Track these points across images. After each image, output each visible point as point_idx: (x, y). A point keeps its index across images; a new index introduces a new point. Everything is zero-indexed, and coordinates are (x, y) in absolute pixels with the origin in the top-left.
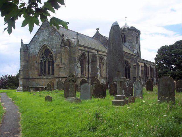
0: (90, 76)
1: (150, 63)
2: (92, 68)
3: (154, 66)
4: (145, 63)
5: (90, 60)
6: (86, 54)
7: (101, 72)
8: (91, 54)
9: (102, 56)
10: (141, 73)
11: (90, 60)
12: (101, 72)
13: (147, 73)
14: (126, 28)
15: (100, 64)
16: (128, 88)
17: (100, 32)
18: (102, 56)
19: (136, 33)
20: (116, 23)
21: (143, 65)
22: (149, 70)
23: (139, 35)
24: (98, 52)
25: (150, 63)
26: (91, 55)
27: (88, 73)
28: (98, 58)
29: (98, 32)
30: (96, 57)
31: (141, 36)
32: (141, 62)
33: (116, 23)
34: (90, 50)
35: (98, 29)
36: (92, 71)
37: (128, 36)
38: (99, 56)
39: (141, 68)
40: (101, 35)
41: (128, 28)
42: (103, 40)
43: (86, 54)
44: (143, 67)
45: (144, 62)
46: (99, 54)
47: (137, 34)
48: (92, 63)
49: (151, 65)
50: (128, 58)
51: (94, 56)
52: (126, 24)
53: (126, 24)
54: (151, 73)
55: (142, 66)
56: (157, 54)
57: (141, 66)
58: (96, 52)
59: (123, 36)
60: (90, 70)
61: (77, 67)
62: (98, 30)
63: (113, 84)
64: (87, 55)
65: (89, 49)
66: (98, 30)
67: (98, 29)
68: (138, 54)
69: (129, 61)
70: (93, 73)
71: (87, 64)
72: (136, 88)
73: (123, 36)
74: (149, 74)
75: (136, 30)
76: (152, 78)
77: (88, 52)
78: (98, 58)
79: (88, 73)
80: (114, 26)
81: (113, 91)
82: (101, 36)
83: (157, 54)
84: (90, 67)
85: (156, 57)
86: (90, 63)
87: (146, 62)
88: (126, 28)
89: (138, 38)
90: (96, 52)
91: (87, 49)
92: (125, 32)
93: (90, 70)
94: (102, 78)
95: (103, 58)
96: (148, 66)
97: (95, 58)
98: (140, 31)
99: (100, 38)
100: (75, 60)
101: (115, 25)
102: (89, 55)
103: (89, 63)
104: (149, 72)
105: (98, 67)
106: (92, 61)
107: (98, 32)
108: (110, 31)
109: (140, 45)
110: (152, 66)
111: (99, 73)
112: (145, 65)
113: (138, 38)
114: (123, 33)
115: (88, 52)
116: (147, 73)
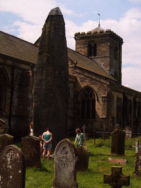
0: (14, 113)
1: (134, 94)
4: (124, 94)
6: (9, 71)
8: (19, 71)
10: (116, 112)
14: (98, 31)
16: (11, 170)
20: (57, 10)
21: (121, 96)
25: (134, 94)
26: (18, 74)
27: (11, 107)
32: (116, 91)
41: (102, 32)
43: (9, 71)
44: (120, 99)
47: (116, 43)
49: (136, 96)
50: (94, 84)
52: (99, 25)
53: (99, 25)
57: (115, 99)
59: (93, 45)
60: (16, 101)
68: (116, 77)
69: (95, 88)
72: (60, 159)
73: (93, 45)
74: (131, 112)
77: (13, 68)
79: (11, 107)
80: (52, 16)
84: (15, 96)
88: (98, 31)
91: (9, 62)
92: (96, 39)
93: (16, 101)
98: (122, 40)
101: (53, 13)
103: (12, 89)
108: (45, 26)
113: (118, 50)
114: (92, 39)
115: (13, 68)
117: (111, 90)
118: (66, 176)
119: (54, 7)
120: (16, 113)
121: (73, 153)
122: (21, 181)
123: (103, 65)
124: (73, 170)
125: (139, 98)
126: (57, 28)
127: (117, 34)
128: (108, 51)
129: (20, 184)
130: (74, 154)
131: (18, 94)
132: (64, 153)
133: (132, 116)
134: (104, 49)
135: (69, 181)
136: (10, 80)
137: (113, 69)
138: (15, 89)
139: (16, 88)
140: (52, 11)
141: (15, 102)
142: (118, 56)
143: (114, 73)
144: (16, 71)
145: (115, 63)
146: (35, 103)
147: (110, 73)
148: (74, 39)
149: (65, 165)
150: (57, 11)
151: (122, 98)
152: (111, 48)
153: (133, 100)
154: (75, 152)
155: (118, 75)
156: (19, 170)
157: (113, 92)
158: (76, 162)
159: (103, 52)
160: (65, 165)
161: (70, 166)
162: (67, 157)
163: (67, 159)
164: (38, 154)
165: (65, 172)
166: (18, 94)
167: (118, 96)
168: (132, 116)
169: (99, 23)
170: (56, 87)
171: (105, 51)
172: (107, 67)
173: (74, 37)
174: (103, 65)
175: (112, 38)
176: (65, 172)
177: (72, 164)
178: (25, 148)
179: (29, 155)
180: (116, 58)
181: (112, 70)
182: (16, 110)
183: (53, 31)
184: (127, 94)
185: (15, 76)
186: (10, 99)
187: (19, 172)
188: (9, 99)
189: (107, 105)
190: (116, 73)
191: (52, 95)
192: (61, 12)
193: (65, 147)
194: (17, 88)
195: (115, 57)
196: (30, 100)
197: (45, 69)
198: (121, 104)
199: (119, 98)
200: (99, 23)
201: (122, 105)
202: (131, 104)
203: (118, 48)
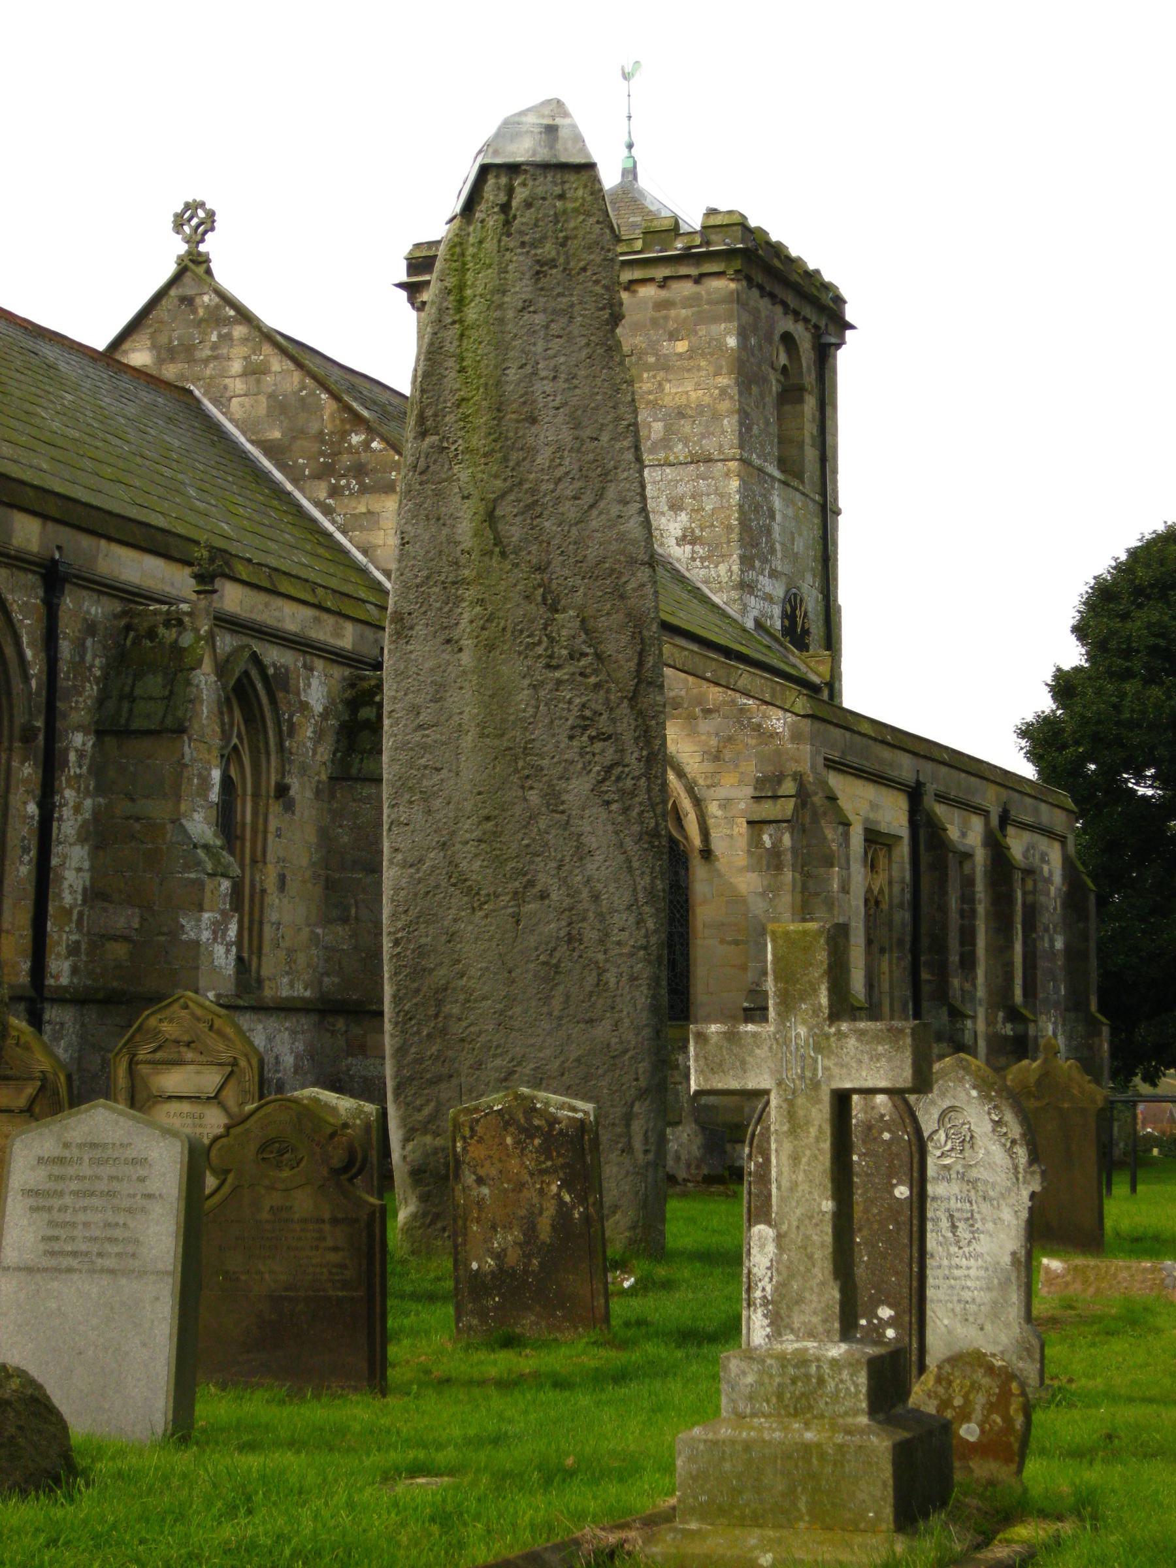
0: (60, 971)
1: (990, 798)
2: (99, 834)
3: (1043, 843)
4: (914, 794)
5: (80, 706)
7: (246, 902)
8: (97, 609)
9: (274, 656)
11: (80, 706)
12: (246, 902)
13: (954, 944)
15: (227, 784)
17: (233, 270)
18: (274, 656)
19: (787, 324)
21: (893, 814)
22: (968, 899)
23: (825, 356)
24: (206, 580)
25: (990, 798)
26: (91, 628)
28: (205, 680)
29: (194, 266)
30: (178, 665)
31: (848, 361)
33: (551, 130)
34: (86, 541)
35: (195, 221)
36: (95, 895)
37: (664, 365)
38: (226, 642)
39: (858, 873)
40: (245, 316)
42: (279, 407)
45: (905, 767)
46: (227, 622)
48: (97, 770)
51: (142, 646)
54: (1009, 946)
55: (875, 839)
56: (1073, 655)
58: (170, 579)
60: (74, 865)
61: (718, 789)
62: (195, 240)
63: (506, 1119)
64: (28, 625)
65: (64, 535)
66: (195, 240)
67: (195, 221)
70: (125, 919)
71: (27, 771)
74: (968, 963)
75: (770, 271)
76: (1014, 1015)
77: (54, 577)
78: (205, 680)
80: (513, 169)
81: (507, 1239)
82: (239, 331)
83: (1073, 655)
84: (68, 825)
85: (1045, 704)
86: (74, 766)
87: (936, 779)
89: (810, 402)
90: (170, 579)
94: (262, 1009)
95: (278, 683)
96: (967, 833)
97: (153, 684)
98: (839, 301)
99: (236, 367)
100: (769, 531)
101: (521, 151)
102: (68, 628)
103: (51, 764)
104: (968, 936)
105: (200, 825)
106: (110, 730)
107: (194, 266)
109: (826, 511)
110: (1017, 844)
111: (219, 929)
112: (925, 831)
113: (810, 402)
115: (54, 577)
116: (940, 946)
117: (820, 761)
118: (967, 1295)
119: (520, 96)
120: (75, 970)
121: (1014, 1142)
122: (911, 1241)
123: (682, 540)
124: (1014, 1254)
125: (1027, 836)
126: (552, 263)
127: (794, 252)
128: (725, 406)
129: (906, 1256)
130: (1021, 1152)
131: (88, 803)
132: (952, 1149)
133: (981, 993)
134: (684, 390)
135: (988, 1327)
136: (34, 683)
137: (774, 574)
138: (66, 762)
139: (72, 756)
140: (509, 129)
141: (70, 876)
142: (811, 454)
143: (777, 611)
144: (82, 608)
145: (785, 516)
146: (405, 865)
147: (744, 610)
148: (404, 294)
149: (954, 1227)
150: (551, 130)
151: (904, 833)
152: (747, 376)
153: (980, 856)
154: (1023, 1135)
155: (811, 625)
156: (895, 1186)
157: (835, 781)
158: (1033, 1196)
159: (681, 415)
160: (954, 1227)
161: (990, 1226)
162: (974, 1173)
163: (973, 1183)
164: (586, 1218)
165: (958, 1267)
166: (88, 803)
167: (872, 816)
168: (981, 993)
169: (630, 146)
170: (571, 738)
171: (700, 409)
172: (715, 555)
173: (403, 277)
174: (682, 540)
175: (755, 292)
176: (958, 1267)
177: (1007, 1215)
178: (480, 1181)
179: (516, 1234)
180: (790, 467)
181: (766, 584)
182: (74, 950)
183: (522, 289)
184: (941, 798)
185: (65, 648)
186: (33, 853)
187: (891, 1193)
188: (26, 850)
189: (798, 897)
190: (792, 606)
191: (534, 797)
192: (578, 138)
193: (952, 1108)
194: (81, 754)
195: (782, 464)
196: (200, 852)
197: (470, 594)
198: (896, 889)
199: (879, 833)
200: (630, 146)
201: (908, 896)
202: (969, 882)
203: (810, 379)
